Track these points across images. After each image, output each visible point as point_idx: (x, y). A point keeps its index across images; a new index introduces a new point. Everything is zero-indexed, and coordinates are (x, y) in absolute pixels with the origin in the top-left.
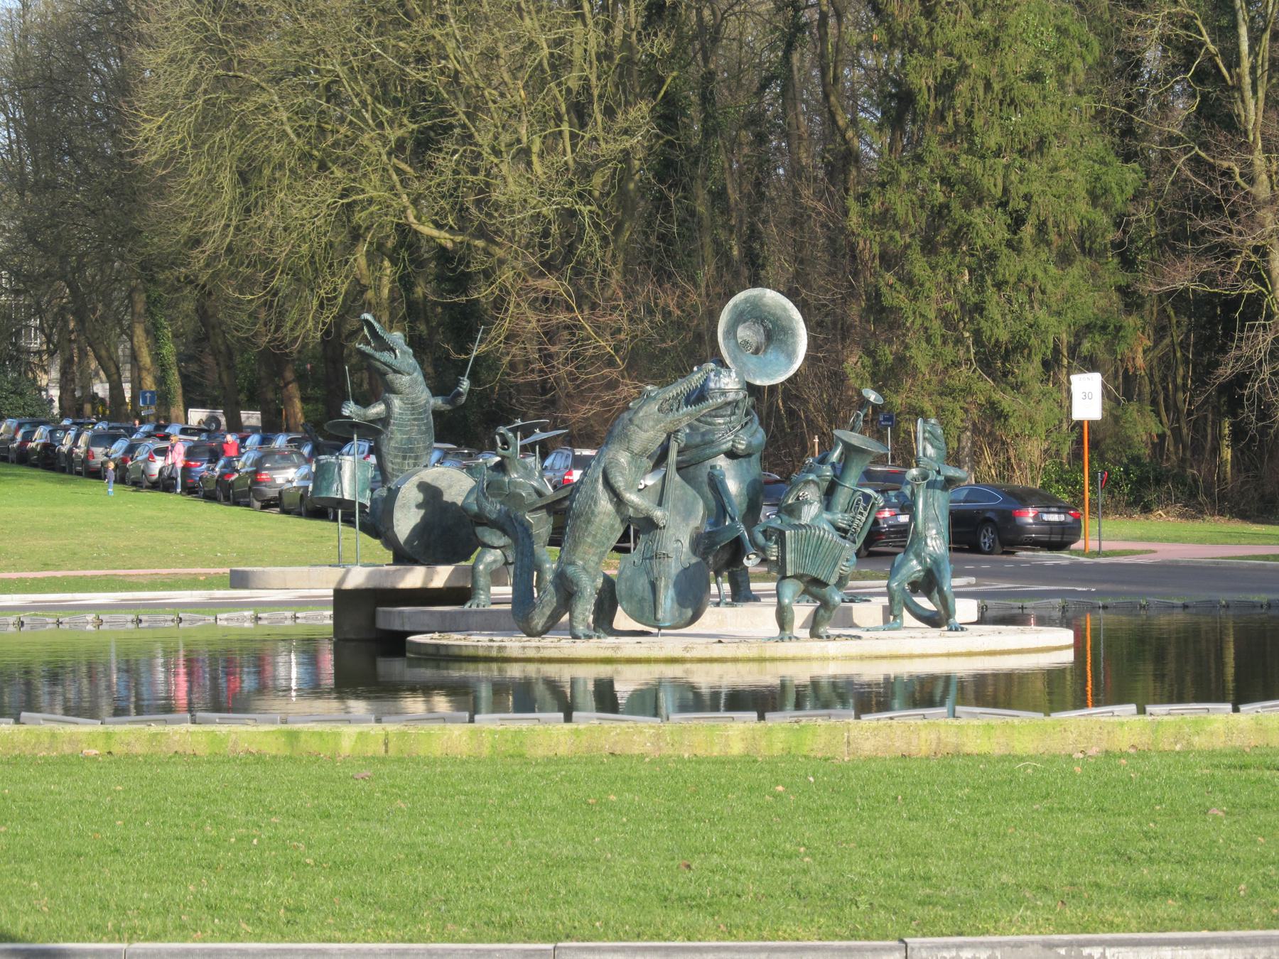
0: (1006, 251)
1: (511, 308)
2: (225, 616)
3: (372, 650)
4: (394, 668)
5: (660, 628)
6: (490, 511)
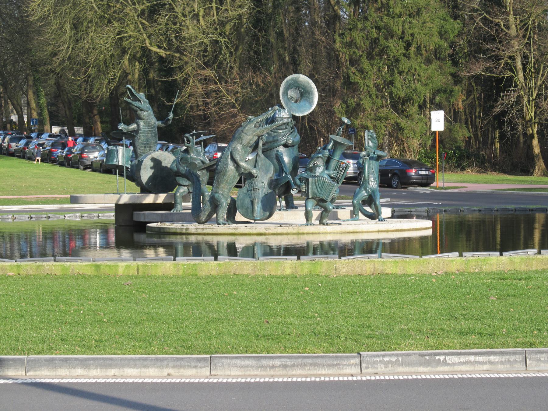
0: (403, 58)
2: (68, 215)
3: (131, 229)
4: (141, 237)
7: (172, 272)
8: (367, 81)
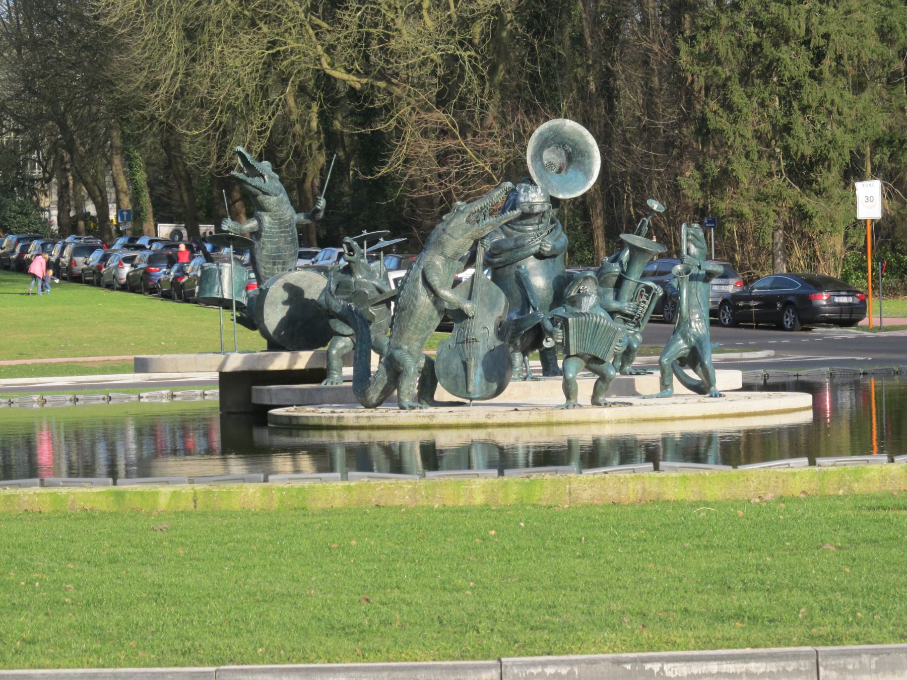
0: (808, 80)
1: (407, 138)
2: (146, 394)
3: (248, 421)
4: (262, 436)
5: (471, 400)
6: (336, 306)
7: (259, 504)
8: (740, 127)
